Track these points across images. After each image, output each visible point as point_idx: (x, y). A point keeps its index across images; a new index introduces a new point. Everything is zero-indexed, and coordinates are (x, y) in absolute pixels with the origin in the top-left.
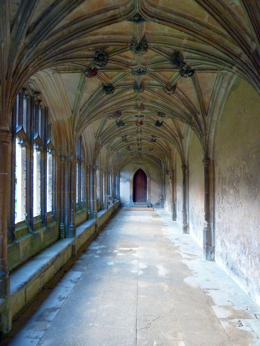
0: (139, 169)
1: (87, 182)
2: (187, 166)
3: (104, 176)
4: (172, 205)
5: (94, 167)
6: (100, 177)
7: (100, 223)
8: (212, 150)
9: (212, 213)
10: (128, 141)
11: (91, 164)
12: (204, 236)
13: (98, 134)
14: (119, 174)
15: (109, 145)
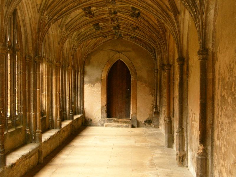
0: (118, 60)
1: (25, 83)
2: (186, 59)
3: (54, 74)
4: (167, 123)
5: (37, 59)
6: (48, 75)
7: (45, 151)
8: (211, 37)
9: (210, 133)
10: (94, 14)
11: (32, 55)
12: (198, 166)
13: (42, 6)
14: (84, 70)
15: (63, 21)
